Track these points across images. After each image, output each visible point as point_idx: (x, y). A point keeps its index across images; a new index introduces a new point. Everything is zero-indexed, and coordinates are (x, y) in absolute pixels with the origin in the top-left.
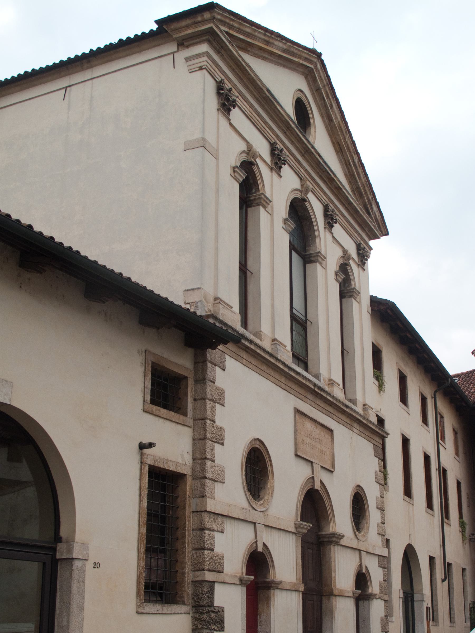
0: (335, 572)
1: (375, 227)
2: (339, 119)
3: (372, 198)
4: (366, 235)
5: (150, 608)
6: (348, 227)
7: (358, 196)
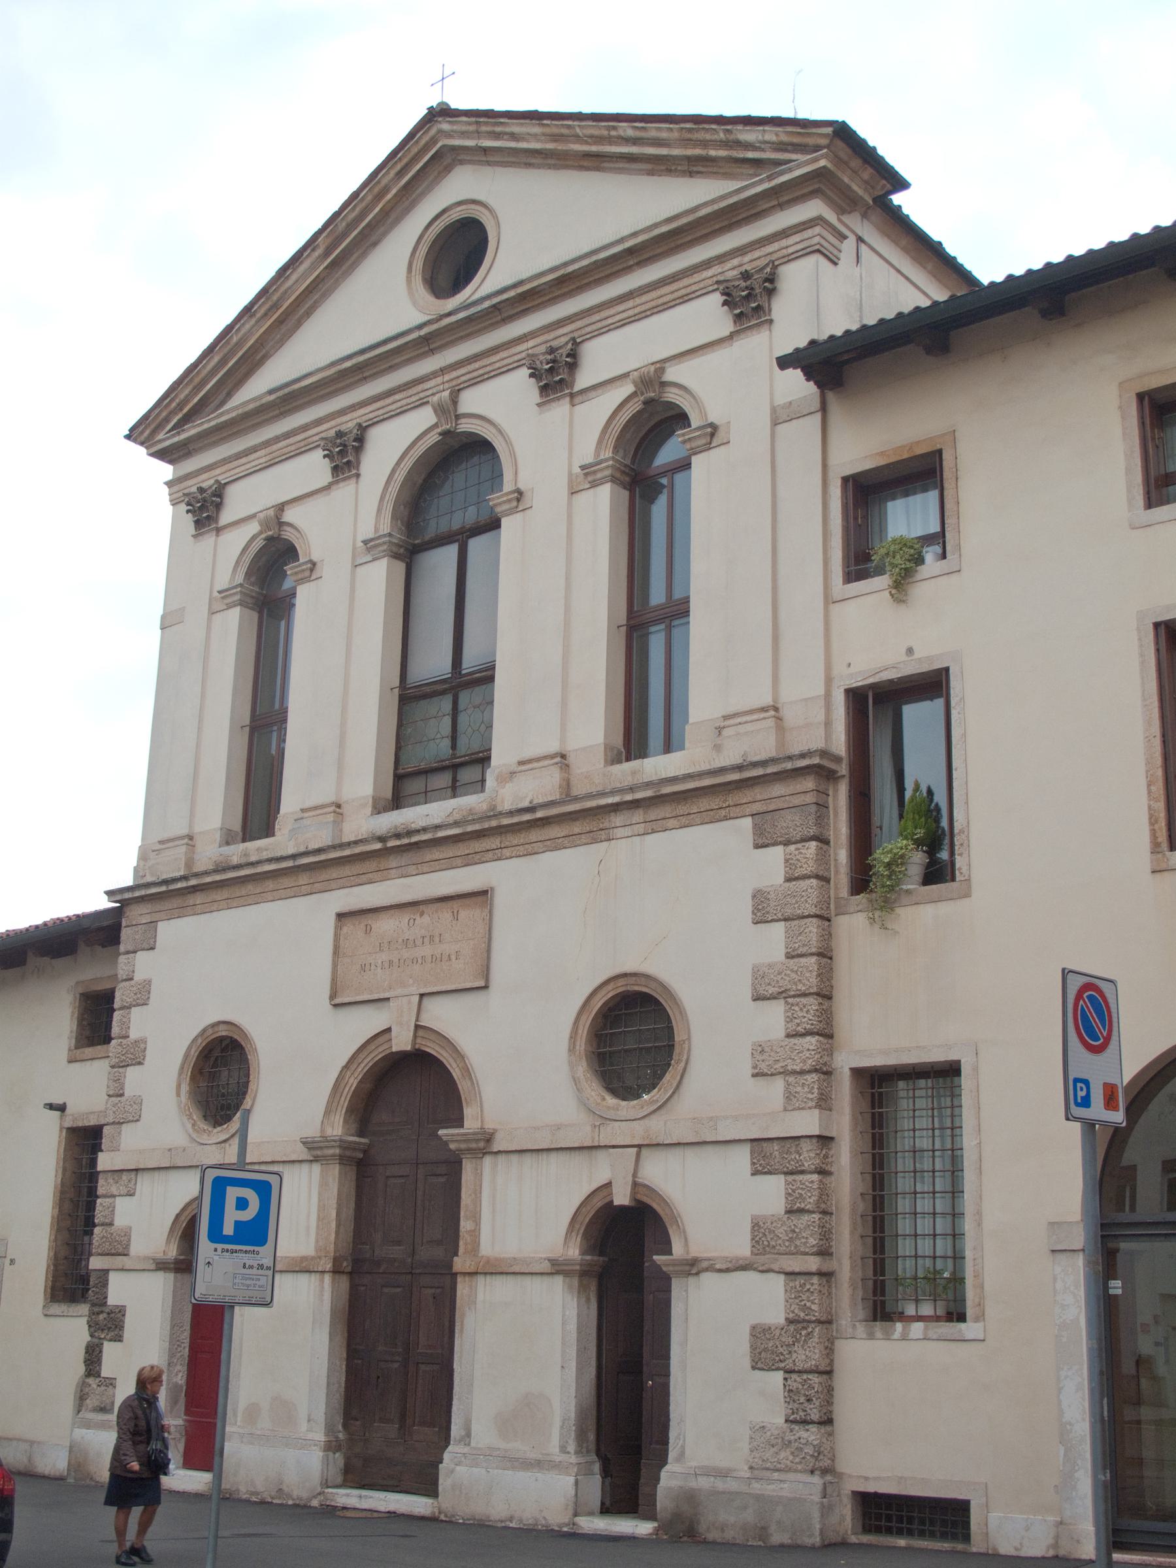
0: (476, 1218)
1: (770, 178)
2: (536, 130)
3: (728, 130)
4: (782, 210)
5: (57, 1308)
6: (672, 292)
7: (707, 166)
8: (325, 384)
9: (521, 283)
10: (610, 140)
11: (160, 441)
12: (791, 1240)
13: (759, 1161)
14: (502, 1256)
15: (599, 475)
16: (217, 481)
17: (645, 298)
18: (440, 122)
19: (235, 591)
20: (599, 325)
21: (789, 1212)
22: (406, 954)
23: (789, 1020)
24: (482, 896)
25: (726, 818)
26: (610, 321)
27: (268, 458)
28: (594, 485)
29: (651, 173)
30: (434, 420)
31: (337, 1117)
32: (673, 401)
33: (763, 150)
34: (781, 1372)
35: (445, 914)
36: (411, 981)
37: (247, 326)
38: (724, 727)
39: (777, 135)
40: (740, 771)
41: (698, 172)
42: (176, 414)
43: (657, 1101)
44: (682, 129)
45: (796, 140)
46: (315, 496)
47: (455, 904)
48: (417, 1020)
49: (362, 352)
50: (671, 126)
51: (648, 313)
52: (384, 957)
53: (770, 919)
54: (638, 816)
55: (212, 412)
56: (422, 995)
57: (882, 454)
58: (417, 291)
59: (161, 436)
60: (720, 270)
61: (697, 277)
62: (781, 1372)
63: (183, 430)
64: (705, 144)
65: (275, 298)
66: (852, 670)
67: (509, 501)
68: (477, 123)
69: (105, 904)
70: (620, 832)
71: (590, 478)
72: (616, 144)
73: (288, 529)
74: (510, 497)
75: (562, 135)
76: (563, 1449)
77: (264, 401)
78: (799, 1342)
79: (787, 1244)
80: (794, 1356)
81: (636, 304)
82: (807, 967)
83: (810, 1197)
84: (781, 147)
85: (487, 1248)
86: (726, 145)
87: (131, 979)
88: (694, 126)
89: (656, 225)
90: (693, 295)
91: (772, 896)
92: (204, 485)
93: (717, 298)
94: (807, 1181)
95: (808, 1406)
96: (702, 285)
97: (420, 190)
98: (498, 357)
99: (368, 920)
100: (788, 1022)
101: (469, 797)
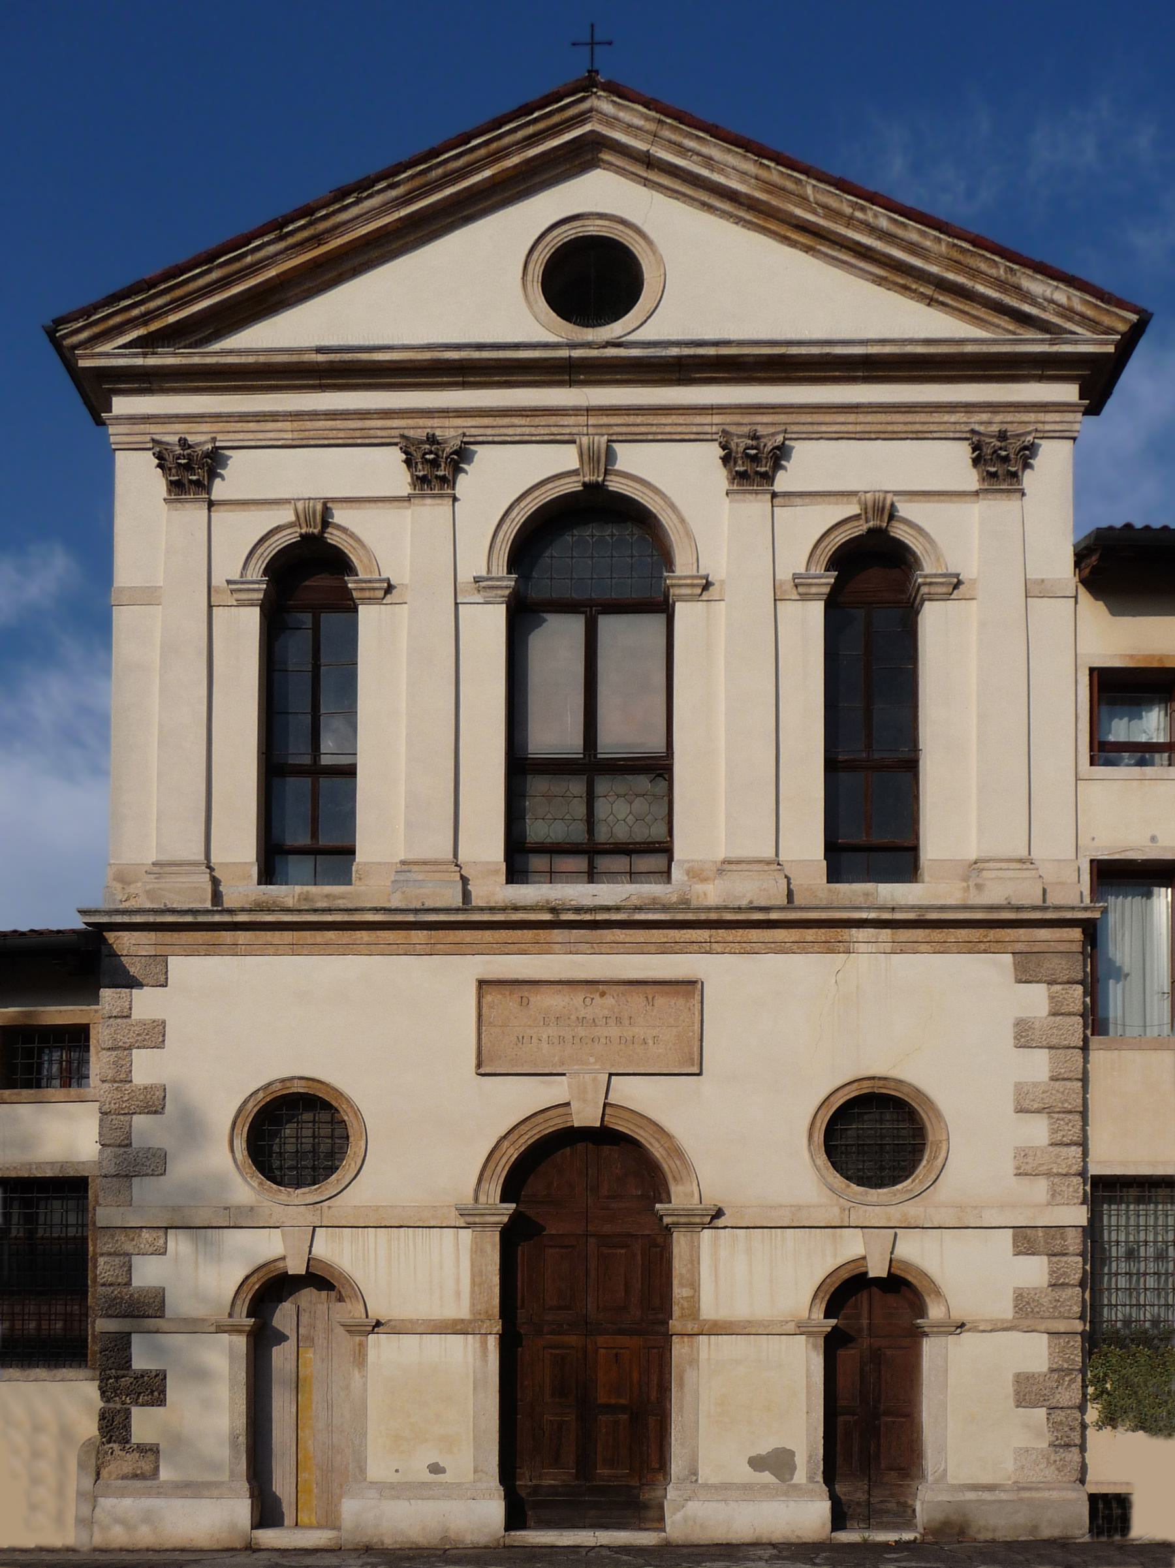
1: (1052, 342)
2: (749, 167)
3: (1011, 270)
6: (905, 423)
8: (300, 371)
9: (727, 343)
10: (850, 221)
11: (107, 355)
12: (1055, 1307)
13: (1023, 1244)
14: (733, 1319)
15: (814, 590)
16: (214, 440)
17: (870, 418)
18: (599, 97)
19: (256, 586)
20: (810, 428)
21: (1052, 1286)
22: (582, 1032)
23: (1054, 1131)
24: (689, 986)
25: (985, 952)
26: (824, 428)
27: (296, 435)
28: (804, 598)
29: (879, 281)
30: (575, 465)
31: (493, 1186)
32: (902, 538)
33: (1044, 309)
34: (1045, 1409)
35: (636, 1000)
36: (592, 1060)
37: (272, 249)
38: (983, 870)
39: (1069, 298)
40: (1017, 912)
41: (943, 304)
42: (136, 327)
43: (911, 1190)
44: (955, 245)
45: (1090, 313)
46: (380, 504)
47: (649, 989)
48: (606, 1098)
49: (480, 347)
50: (942, 236)
51: (873, 436)
52: (551, 1031)
53: (1034, 1045)
54: (886, 934)
55: (185, 348)
56: (611, 1075)
57: (1132, 657)
58: (537, 302)
59: (107, 347)
60: (965, 419)
61: (936, 417)
62: (1045, 1409)
63: (153, 353)
64: (975, 273)
65: (322, 226)
66: (1095, 843)
67: (693, 586)
68: (660, 121)
69: (78, 923)
70: (862, 947)
71: (801, 590)
72: (856, 229)
73: (335, 532)
74: (696, 582)
75: (783, 189)
76: (811, 1479)
77: (306, 358)
78: (1062, 1384)
79: (1051, 1310)
80: (1058, 1396)
81: (858, 420)
82: (1074, 1090)
83: (1074, 1274)
84: (1067, 312)
85: (709, 1310)
86: (1000, 286)
87: (129, 1017)
88: (971, 248)
89: (912, 341)
90: (930, 436)
91: (1037, 1025)
92: (191, 439)
93: (714, 451)
94: (1071, 1261)
95: (1072, 1434)
96: (942, 428)
97: (545, 177)
98: (669, 420)
99: (525, 991)
100: (1052, 1133)
101: (653, 885)
